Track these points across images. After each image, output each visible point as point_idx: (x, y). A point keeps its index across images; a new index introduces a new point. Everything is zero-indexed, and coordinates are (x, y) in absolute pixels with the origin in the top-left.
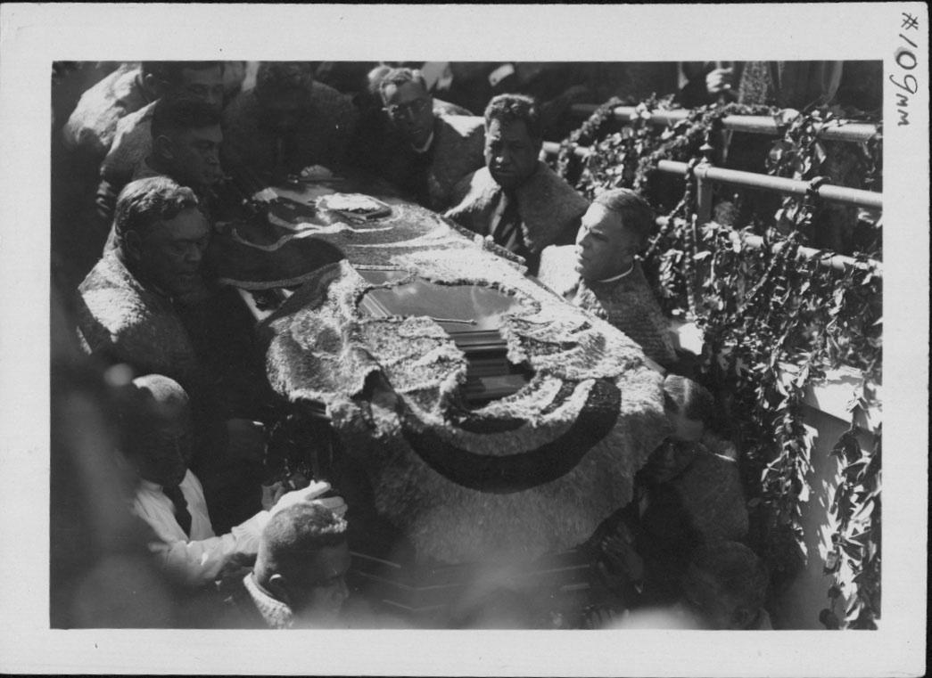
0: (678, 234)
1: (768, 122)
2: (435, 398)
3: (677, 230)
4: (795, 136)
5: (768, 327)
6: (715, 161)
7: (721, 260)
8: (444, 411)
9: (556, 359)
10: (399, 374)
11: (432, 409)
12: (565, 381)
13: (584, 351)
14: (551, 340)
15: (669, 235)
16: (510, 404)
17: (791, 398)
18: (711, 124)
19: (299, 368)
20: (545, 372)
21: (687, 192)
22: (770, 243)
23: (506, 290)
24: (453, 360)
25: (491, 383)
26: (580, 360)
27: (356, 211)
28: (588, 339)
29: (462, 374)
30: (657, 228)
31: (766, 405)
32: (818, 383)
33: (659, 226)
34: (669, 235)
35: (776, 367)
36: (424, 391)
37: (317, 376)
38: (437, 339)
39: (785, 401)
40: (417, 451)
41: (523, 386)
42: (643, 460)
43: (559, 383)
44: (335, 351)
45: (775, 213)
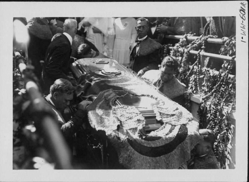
0: (195, 70)
1: (220, 40)
2: (136, 131)
3: (195, 69)
4: (227, 44)
5: (220, 96)
6: (206, 51)
7: (207, 78)
8: (139, 135)
9: (169, 119)
10: (126, 123)
11: (135, 134)
12: (172, 125)
13: (177, 117)
14: (168, 114)
15: (193, 71)
16: (157, 132)
17: (226, 115)
18: (204, 41)
19: (98, 121)
20: (166, 123)
21: (198, 59)
22: (221, 73)
23: (155, 98)
24: (141, 120)
25: (151, 126)
26: (176, 119)
27: (112, 73)
28: (178, 113)
29: (144, 124)
30: (189, 69)
31: (219, 117)
32: (234, 112)
33: (190, 68)
34: (193, 71)
35: (222, 107)
36: (133, 129)
37: (103, 124)
38: (137, 113)
39: (225, 116)
40: (132, 146)
41: (161, 127)
42: (193, 147)
43: (170, 126)
44: (108, 116)
45: (222, 65)
